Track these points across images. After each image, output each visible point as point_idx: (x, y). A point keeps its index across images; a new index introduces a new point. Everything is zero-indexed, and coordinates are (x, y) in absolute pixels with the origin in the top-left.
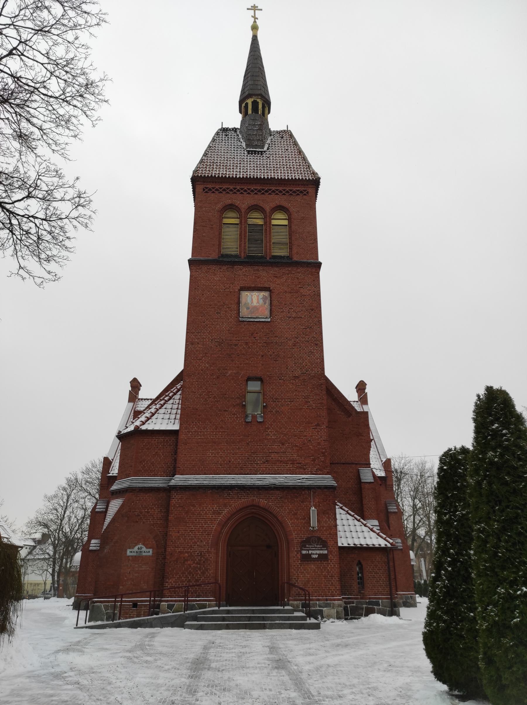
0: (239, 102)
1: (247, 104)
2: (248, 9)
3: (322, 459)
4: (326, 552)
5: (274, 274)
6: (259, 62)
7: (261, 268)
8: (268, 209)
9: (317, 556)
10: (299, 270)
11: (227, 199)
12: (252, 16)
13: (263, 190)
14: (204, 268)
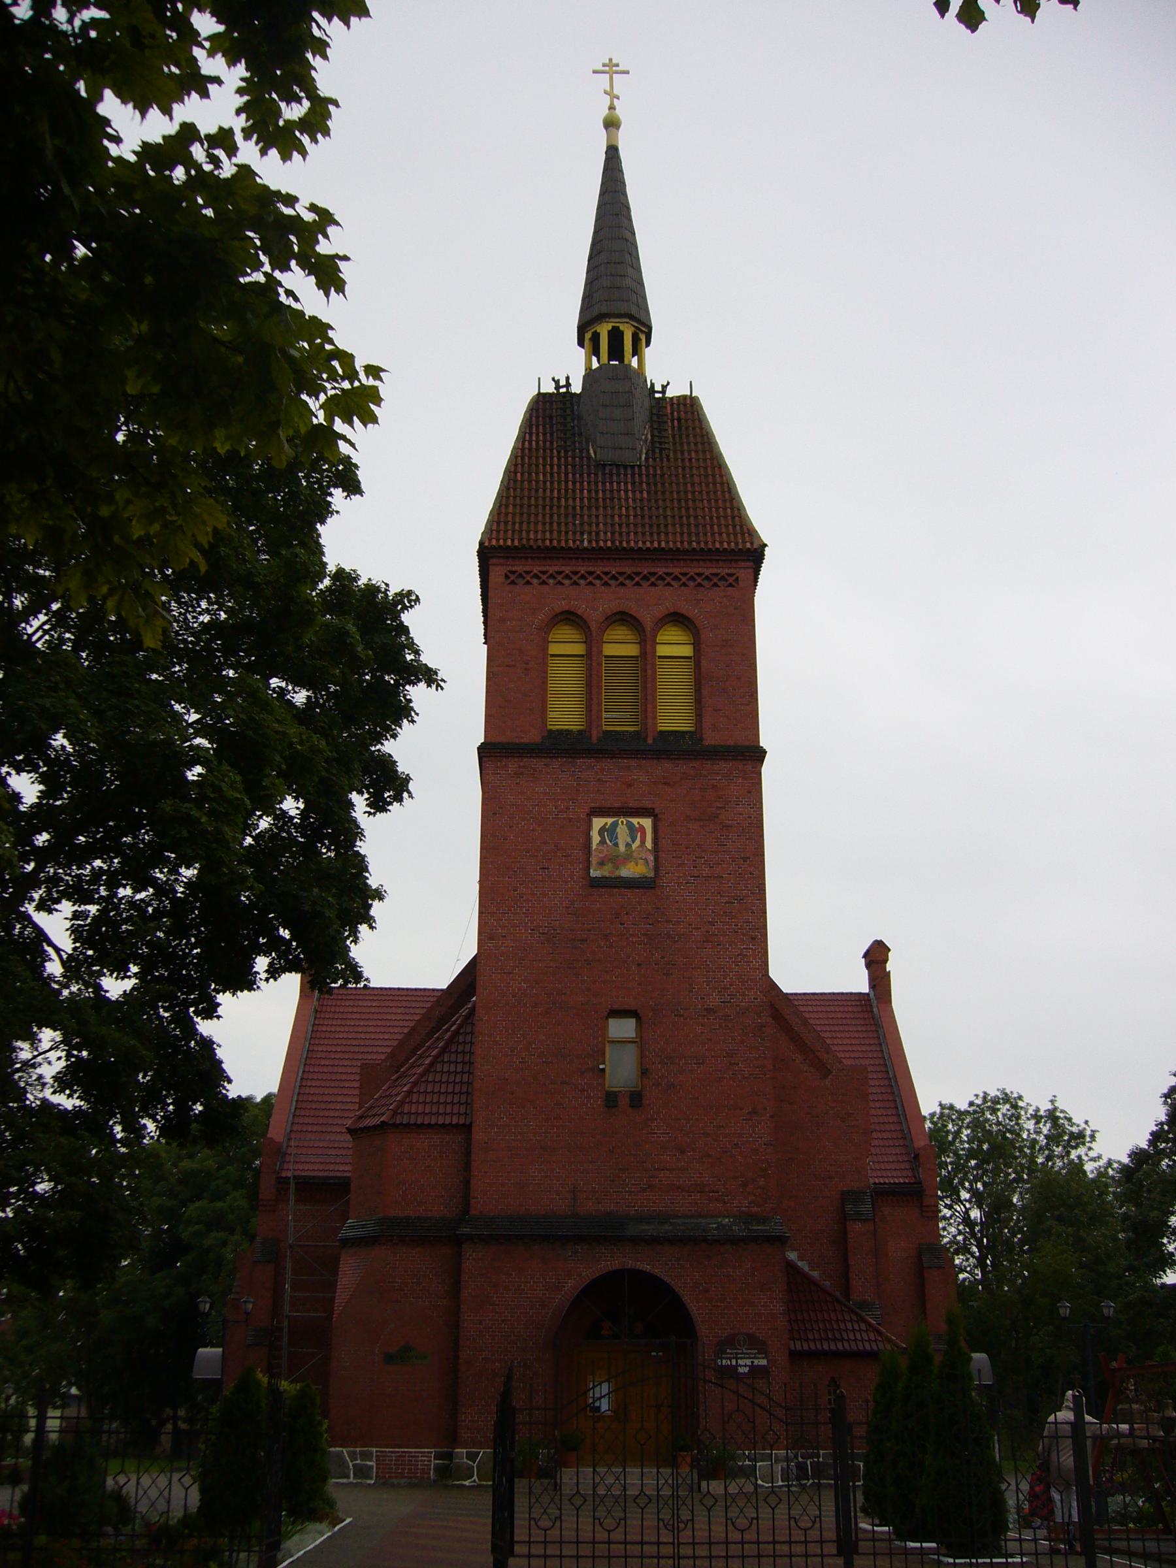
0: (579, 328)
1: (596, 338)
2: (595, 72)
3: (762, 1182)
4: (764, 1362)
5: (664, 777)
6: (628, 235)
7: (634, 763)
8: (648, 622)
9: (746, 1370)
10: (716, 767)
11: (561, 598)
12: (606, 92)
13: (637, 574)
14: (513, 765)
